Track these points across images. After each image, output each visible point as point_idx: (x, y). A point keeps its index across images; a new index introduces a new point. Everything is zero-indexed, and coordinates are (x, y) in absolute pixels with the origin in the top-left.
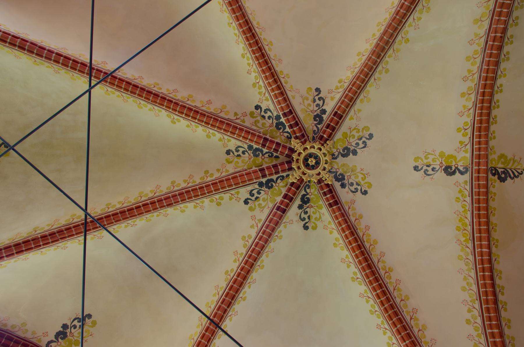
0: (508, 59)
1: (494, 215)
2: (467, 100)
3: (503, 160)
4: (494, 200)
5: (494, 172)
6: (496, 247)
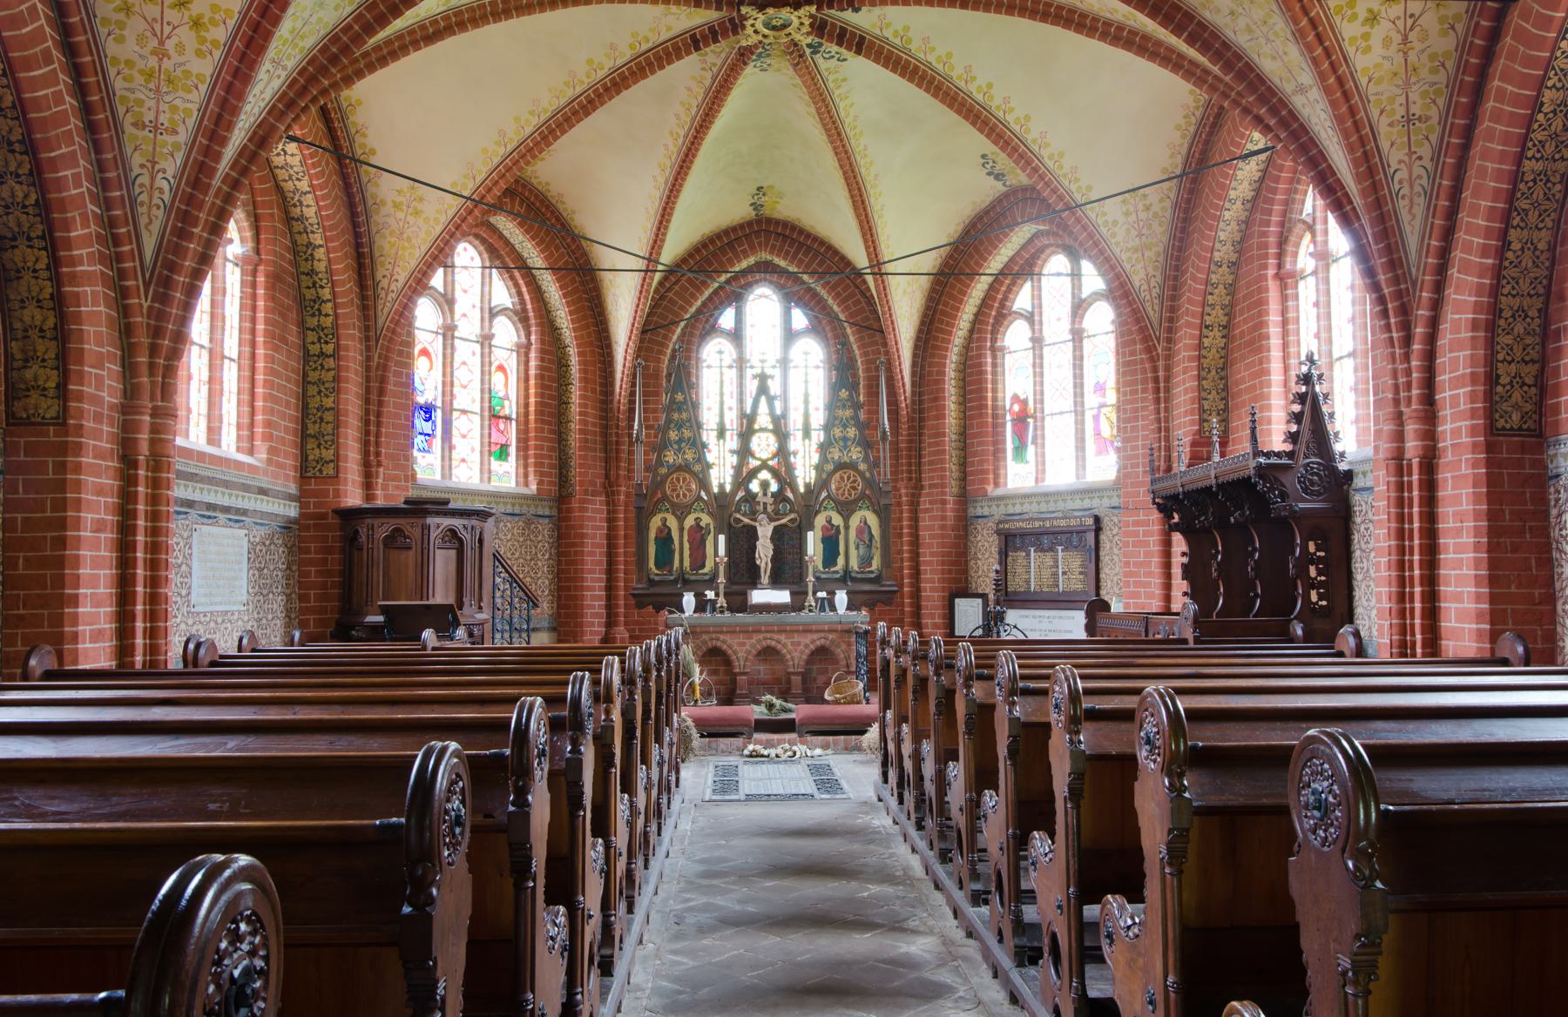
2: (979, 87)
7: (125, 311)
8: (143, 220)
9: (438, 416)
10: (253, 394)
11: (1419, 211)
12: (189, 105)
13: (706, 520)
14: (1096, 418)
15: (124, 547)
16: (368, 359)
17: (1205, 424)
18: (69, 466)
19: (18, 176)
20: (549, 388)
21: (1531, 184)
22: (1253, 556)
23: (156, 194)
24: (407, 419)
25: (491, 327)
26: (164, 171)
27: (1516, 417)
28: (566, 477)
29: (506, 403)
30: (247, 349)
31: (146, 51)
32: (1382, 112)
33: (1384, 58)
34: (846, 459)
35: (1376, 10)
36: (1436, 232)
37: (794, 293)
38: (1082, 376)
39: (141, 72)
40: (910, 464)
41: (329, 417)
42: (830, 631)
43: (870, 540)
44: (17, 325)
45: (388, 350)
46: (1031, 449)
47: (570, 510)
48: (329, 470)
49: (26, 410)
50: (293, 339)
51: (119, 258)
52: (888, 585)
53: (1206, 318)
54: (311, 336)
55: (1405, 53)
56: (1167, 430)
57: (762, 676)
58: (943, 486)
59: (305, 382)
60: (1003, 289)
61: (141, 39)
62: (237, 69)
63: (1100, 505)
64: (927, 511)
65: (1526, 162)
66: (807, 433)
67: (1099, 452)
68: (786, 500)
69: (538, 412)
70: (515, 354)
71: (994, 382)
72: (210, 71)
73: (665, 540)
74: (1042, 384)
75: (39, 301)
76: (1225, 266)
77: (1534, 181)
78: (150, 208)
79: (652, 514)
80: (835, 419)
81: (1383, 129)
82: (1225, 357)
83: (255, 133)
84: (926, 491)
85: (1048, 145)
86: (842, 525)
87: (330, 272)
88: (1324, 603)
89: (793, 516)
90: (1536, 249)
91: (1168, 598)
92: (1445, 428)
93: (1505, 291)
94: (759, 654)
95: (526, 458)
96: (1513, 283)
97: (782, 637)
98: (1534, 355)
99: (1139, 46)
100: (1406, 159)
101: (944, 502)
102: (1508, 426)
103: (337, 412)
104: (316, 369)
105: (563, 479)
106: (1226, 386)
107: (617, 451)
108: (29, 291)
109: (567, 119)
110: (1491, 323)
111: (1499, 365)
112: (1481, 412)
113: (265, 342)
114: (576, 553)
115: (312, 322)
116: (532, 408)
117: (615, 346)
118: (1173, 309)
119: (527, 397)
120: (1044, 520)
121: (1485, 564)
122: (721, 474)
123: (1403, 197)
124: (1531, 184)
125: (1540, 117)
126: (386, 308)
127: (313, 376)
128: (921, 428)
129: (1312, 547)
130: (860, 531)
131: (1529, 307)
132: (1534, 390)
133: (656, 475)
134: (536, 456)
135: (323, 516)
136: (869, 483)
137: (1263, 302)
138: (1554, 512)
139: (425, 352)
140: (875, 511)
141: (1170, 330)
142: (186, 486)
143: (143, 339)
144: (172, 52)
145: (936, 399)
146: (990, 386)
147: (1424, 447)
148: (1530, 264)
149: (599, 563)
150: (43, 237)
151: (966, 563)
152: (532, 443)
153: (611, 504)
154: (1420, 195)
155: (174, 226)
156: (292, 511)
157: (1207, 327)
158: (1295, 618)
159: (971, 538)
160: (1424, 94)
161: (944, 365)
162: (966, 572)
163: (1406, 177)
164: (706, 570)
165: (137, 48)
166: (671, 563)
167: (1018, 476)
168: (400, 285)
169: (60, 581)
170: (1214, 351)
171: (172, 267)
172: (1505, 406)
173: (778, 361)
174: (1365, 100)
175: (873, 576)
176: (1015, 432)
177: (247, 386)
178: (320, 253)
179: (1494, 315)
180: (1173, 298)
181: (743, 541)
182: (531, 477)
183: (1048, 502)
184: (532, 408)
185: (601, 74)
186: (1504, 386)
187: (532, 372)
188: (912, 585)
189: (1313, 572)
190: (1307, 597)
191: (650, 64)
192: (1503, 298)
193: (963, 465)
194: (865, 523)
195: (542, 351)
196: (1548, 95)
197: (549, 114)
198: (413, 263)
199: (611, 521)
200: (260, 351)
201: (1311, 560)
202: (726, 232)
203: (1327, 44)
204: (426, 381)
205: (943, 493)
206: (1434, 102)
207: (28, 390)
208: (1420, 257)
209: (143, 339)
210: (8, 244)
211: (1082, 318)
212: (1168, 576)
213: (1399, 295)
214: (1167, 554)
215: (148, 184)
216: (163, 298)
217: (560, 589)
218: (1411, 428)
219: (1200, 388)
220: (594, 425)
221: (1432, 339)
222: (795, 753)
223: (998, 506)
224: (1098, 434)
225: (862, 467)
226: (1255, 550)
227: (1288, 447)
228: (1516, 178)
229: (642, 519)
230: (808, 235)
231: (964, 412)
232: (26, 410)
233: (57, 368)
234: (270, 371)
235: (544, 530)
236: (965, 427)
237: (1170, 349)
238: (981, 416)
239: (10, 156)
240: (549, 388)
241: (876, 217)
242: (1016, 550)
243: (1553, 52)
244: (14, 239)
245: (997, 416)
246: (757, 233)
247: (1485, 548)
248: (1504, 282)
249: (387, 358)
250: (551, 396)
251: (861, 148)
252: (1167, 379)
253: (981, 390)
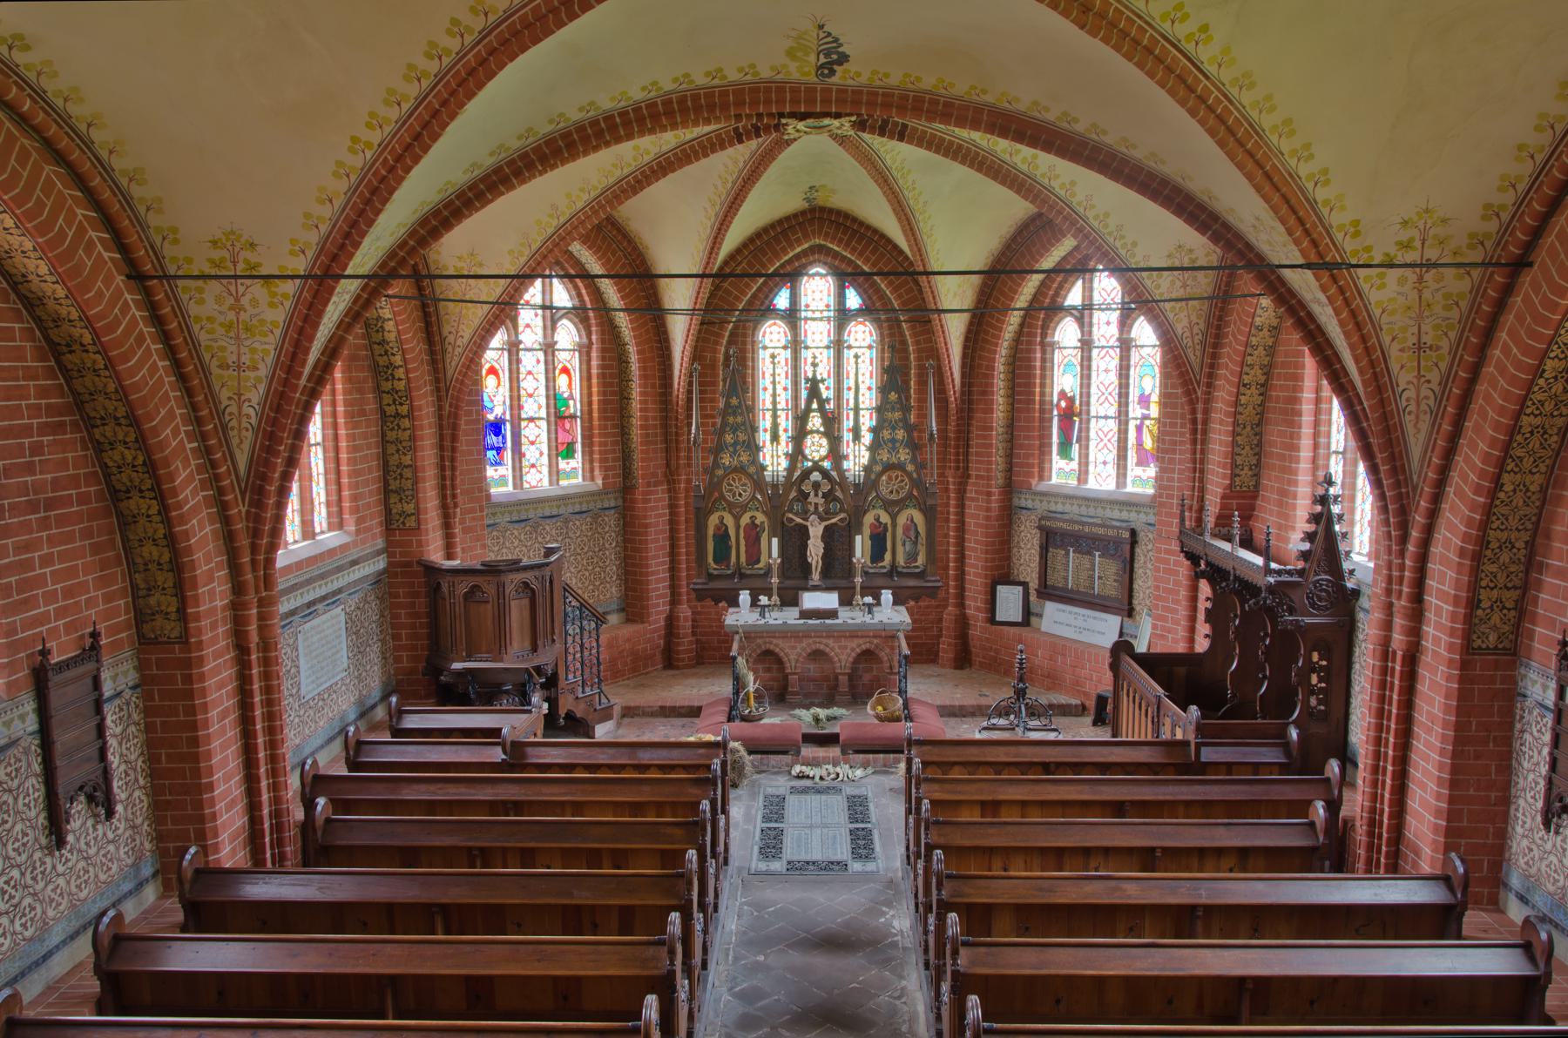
0: (592, 103)
1: (919, 79)
2: (1025, 158)
3: (799, 54)
4: (887, 75)
5: (826, 71)
6: (984, 92)
7: (226, 521)
8: (235, 441)
9: (508, 429)
10: (338, 472)
11: (1425, 426)
12: (266, 346)
13: (761, 518)
14: (1139, 429)
15: (246, 721)
16: (440, 408)
17: (1237, 479)
18: (194, 677)
19: (125, 443)
20: (611, 385)
21: (1528, 435)
22: (1264, 641)
23: (244, 419)
24: (479, 454)
25: (553, 336)
26: (250, 401)
27: (1493, 638)
28: (630, 469)
29: (571, 402)
30: (330, 432)
31: (224, 308)
32: (1393, 339)
33: (1399, 293)
34: (894, 460)
35: (1392, 254)
36: (1438, 450)
37: (845, 276)
38: (1127, 386)
39: (221, 324)
40: (958, 454)
41: (408, 473)
42: (875, 637)
43: (917, 537)
44: (139, 560)
45: (458, 399)
46: (1076, 447)
47: (633, 501)
48: (411, 522)
49: (153, 631)
50: (371, 406)
51: (217, 478)
52: (933, 581)
53: (1245, 377)
54: (387, 399)
55: (1420, 291)
56: (1202, 471)
57: (812, 674)
58: (989, 478)
59: (384, 442)
60: (1055, 285)
61: (219, 300)
62: (307, 316)
63: (1138, 519)
64: (973, 499)
65: (1524, 418)
66: (857, 436)
67: (1140, 463)
68: (836, 499)
69: (602, 410)
70: (577, 354)
71: (1043, 377)
72: (283, 317)
73: (722, 537)
74: (1089, 386)
75: (154, 540)
76: (1265, 330)
77: (1532, 433)
78: (240, 431)
79: (711, 512)
80: (885, 421)
81: (1394, 352)
82: (1262, 414)
83: (326, 347)
84: (972, 480)
85: (1093, 207)
86: (889, 522)
87: (399, 341)
88: (1322, 708)
89: (843, 515)
90: (1528, 490)
91: (1191, 640)
92: (1429, 630)
93: (1494, 526)
94: (810, 655)
95: (591, 453)
96: (1503, 519)
97: (831, 642)
98: (1517, 582)
100: (1415, 381)
101: (989, 494)
102: (1484, 646)
103: (415, 468)
104: (392, 429)
105: (627, 472)
106: (1260, 441)
107: (677, 442)
108: (146, 532)
109: (616, 197)
110: (1478, 553)
111: (1482, 590)
112: (1460, 633)
113: (346, 423)
114: (641, 542)
115: (387, 386)
116: (595, 406)
117: (672, 343)
118: (1214, 356)
119: (590, 395)
120: (1083, 524)
121: (1448, 769)
122: (774, 460)
123: (1410, 413)
124: (1528, 435)
125: (1541, 382)
126: (454, 362)
127: (391, 436)
128: (970, 418)
129: (1315, 656)
130: (906, 529)
131: (1517, 540)
132: (1513, 613)
133: (712, 475)
134: (600, 452)
135: (409, 564)
136: (917, 483)
137: (1298, 378)
138: (1518, 726)
139: (492, 371)
140: (920, 510)
141: (1211, 375)
142: (288, 600)
143: (244, 542)
144: (247, 306)
145: (984, 393)
146: (1038, 381)
147: (1409, 643)
148: (1521, 503)
149: (663, 548)
150: (152, 489)
151: (1009, 550)
152: (596, 440)
153: (672, 491)
154: (1426, 413)
155: (262, 444)
156: (380, 564)
157: (1245, 385)
158: (1293, 722)
159: (1015, 527)
160: (1436, 327)
161: (993, 360)
162: (1009, 558)
163: (1414, 396)
164: (761, 565)
165: (216, 307)
166: (728, 557)
167: (1061, 471)
168: (465, 341)
169: (197, 773)
170: (1250, 408)
171: (264, 478)
172: (1483, 628)
173: (831, 342)
174: (1377, 328)
175: (917, 570)
176: (1061, 428)
177: (333, 466)
178: (390, 326)
179: (1481, 547)
180: (1216, 346)
181: (795, 540)
182: (597, 472)
183: (1088, 507)
184: (595, 406)
185: (647, 158)
186: (1484, 610)
187: (594, 371)
188: (956, 569)
189: (1314, 679)
190: (1306, 702)
191: (688, 157)
192: (1492, 532)
193: (1010, 456)
194: (912, 520)
195: (603, 350)
196: (1549, 365)
197: (598, 192)
198: (477, 322)
199: (673, 507)
200: (342, 432)
201: (1311, 668)
202: (780, 222)
203: (1341, 283)
204: (495, 397)
205: (989, 486)
206: (1446, 334)
207: (153, 614)
208: (1422, 467)
209: (244, 542)
210: (123, 496)
211: (1131, 327)
212: (1193, 619)
213: (1399, 497)
214: (1194, 599)
215: (236, 412)
216: (258, 503)
217: (627, 573)
218: (1398, 621)
219: (1234, 444)
220: (654, 418)
221: (1425, 543)
222: (838, 775)
223: (1041, 501)
224: (1140, 443)
225: (910, 468)
226: (1266, 635)
227: (1300, 565)
228: (1513, 430)
229: (701, 516)
230: (861, 224)
231: (1012, 404)
232: (153, 631)
233: (176, 595)
234: (353, 449)
235: (611, 520)
236: (1012, 419)
237: (1209, 393)
238: (1028, 410)
239: (117, 428)
240: (611, 385)
241: (925, 237)
242: (1056, 547)
243: (1557, 330)
244: (128, 491)
245: (1045, 412)
246: (811, 221)
247: (1450, 755)
248: (1494, 518)
249: (457, 407)
250: (613, 393)
251: (910, 183)
252: (1205, 422)
253: (1030, 385)
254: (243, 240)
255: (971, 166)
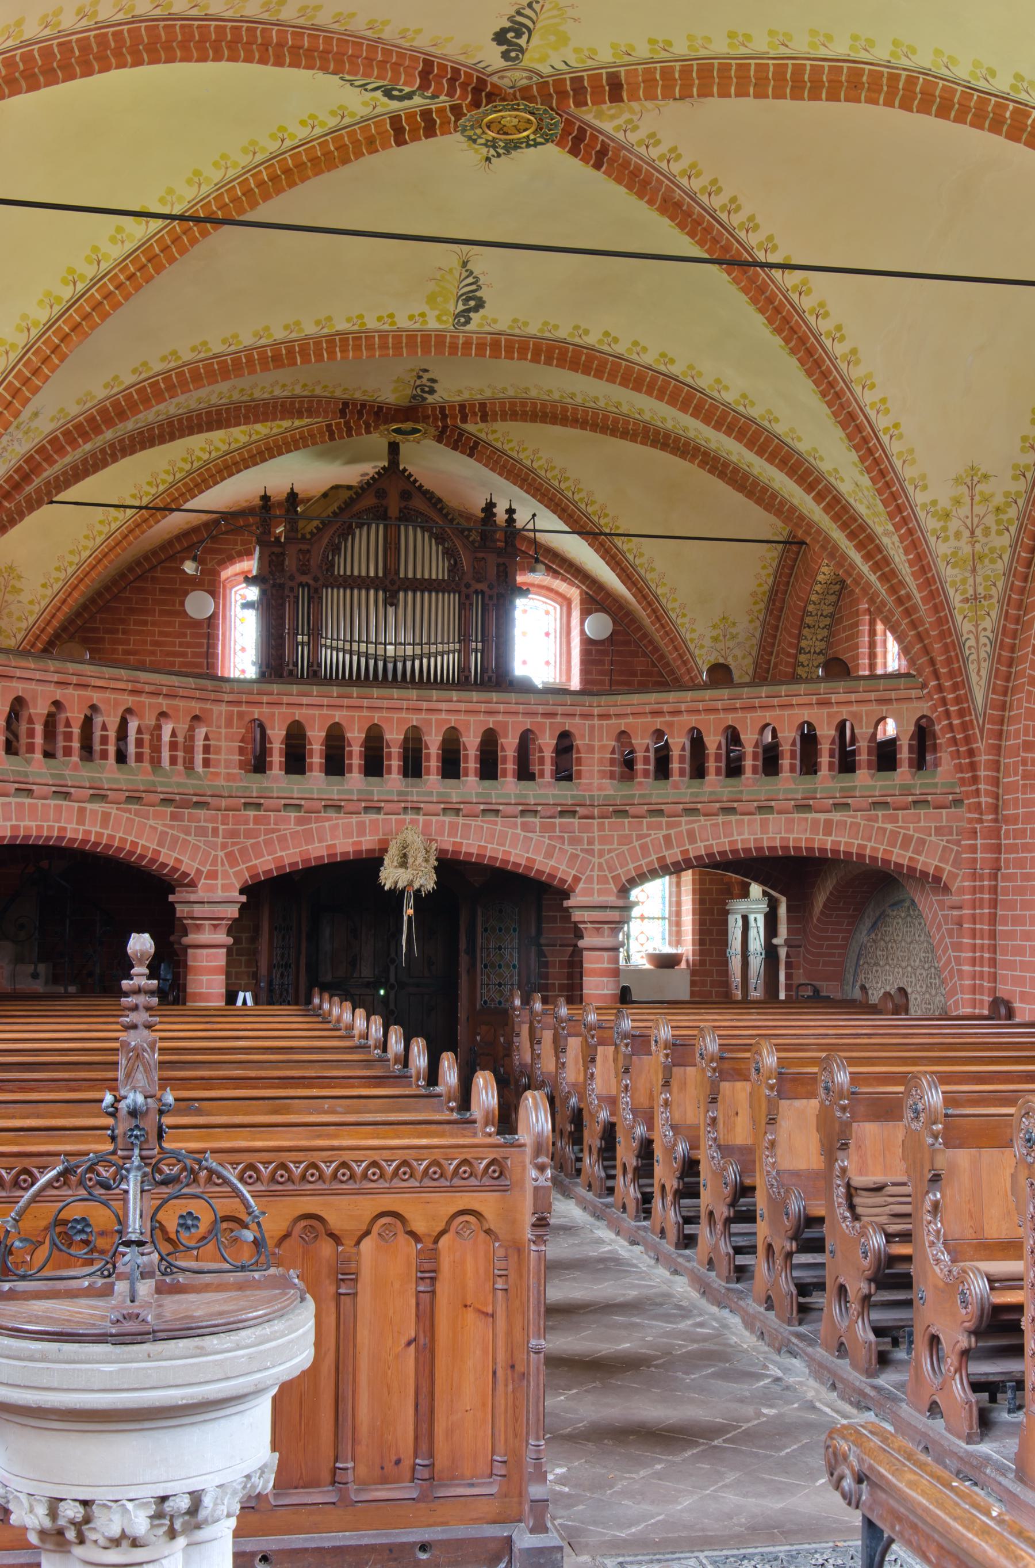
4: (556, 327)
5: (462, 320)
99: (730, 478)
215: (974, 644)
254: (979, 473)
255: (143, 448)
